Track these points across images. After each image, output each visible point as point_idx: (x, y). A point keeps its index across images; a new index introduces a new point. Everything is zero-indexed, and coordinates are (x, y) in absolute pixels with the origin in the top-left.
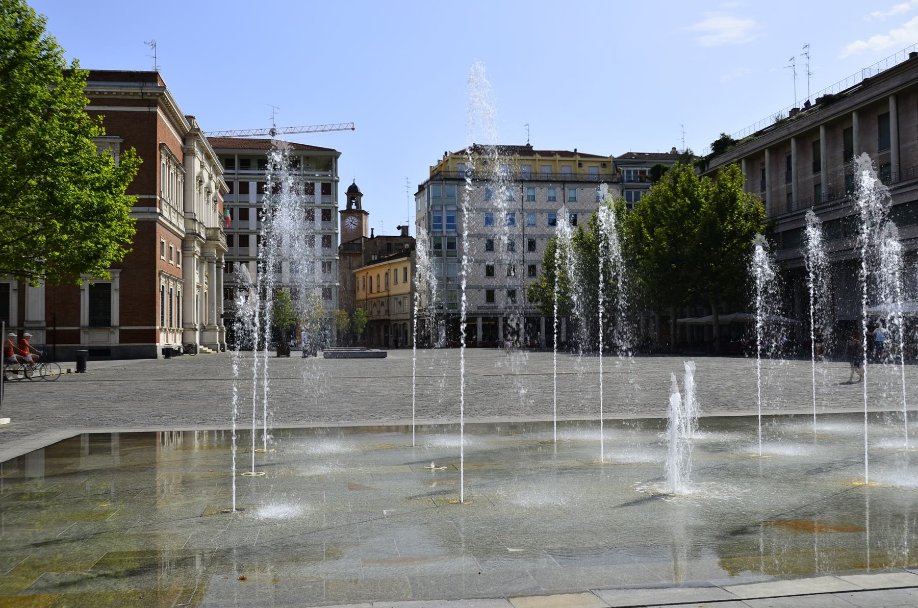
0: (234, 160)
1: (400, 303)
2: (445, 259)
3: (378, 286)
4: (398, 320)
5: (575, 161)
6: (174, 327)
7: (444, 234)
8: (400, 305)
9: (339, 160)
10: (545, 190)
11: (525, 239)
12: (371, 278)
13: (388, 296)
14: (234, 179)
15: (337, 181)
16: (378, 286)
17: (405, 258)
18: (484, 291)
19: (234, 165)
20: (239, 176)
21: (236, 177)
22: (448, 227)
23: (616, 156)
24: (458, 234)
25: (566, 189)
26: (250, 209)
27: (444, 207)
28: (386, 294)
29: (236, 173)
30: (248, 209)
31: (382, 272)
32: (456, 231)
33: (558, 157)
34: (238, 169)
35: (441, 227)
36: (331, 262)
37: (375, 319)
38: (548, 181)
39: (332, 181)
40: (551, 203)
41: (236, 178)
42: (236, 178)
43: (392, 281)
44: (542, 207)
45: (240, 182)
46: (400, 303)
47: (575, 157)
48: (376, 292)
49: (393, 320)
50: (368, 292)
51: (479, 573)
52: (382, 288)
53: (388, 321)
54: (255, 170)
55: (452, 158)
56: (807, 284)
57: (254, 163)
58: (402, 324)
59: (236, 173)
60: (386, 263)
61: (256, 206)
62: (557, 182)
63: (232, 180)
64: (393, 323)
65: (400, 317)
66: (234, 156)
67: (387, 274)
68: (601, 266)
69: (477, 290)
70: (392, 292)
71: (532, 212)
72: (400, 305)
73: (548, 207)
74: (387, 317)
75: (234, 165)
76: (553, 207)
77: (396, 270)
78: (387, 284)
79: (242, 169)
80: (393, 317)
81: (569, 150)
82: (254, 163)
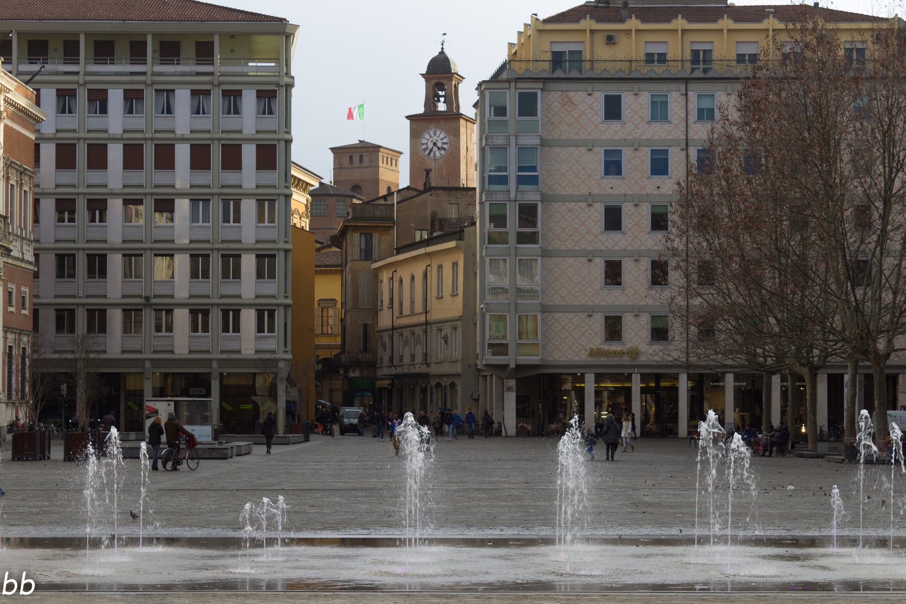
0: (145, 43)
1: (446, 339)
2: (513, 251)
3: (412, 302)
4: (440, 376)
5: (768, 30)
7: (513, 196)
8: (446, 342)
12: (401, 281)
13: (427, 323)
14: (145, 83)
15: (289, 86)
16: (412, 302)
17: (452, 244)
18: (599, 318)
19: (78, 55)
20: (88, 78)
21: (81, 79)
22: (521, 180)
23: (737, 5)
24: (542, 195)
25: (690, 93)
26: (109, 146)
27: (513, 139)
28: (422, 319)
29: (149, 72)
30: (106, 145)
31: (418, 270)
33: (772, 23)
34: (153, 64)
35: (504, 180)
36: (274, 256)
37: (406, 371)
39: (278, 85)
41: (81, 82)
42: (81, 82)
43: (433, 292)
45: (89, 90)
46: (446, 339)
47: (766, 21)
48: (408, 313)
49: (435, 376)
50: (396, 314)
52: (419, 307)
53: (426, 376)
54: (188, 64)
55: (540, 31)
57: (123, 49)
58: (448, 383)
60: (421, 251)
61: (122, 139)
64: (433, 383)
65: (446, 369)
67: (425, 275)
68: (164, 438)
69: (583, 316)
70: (434, 316)
72: (446, 342)
74: (424, 369)
75: (145, 55)
77: (440, 267)
78: (425, 300)
80: (434, 370)
81: (747, 5)
82: (123, 49)
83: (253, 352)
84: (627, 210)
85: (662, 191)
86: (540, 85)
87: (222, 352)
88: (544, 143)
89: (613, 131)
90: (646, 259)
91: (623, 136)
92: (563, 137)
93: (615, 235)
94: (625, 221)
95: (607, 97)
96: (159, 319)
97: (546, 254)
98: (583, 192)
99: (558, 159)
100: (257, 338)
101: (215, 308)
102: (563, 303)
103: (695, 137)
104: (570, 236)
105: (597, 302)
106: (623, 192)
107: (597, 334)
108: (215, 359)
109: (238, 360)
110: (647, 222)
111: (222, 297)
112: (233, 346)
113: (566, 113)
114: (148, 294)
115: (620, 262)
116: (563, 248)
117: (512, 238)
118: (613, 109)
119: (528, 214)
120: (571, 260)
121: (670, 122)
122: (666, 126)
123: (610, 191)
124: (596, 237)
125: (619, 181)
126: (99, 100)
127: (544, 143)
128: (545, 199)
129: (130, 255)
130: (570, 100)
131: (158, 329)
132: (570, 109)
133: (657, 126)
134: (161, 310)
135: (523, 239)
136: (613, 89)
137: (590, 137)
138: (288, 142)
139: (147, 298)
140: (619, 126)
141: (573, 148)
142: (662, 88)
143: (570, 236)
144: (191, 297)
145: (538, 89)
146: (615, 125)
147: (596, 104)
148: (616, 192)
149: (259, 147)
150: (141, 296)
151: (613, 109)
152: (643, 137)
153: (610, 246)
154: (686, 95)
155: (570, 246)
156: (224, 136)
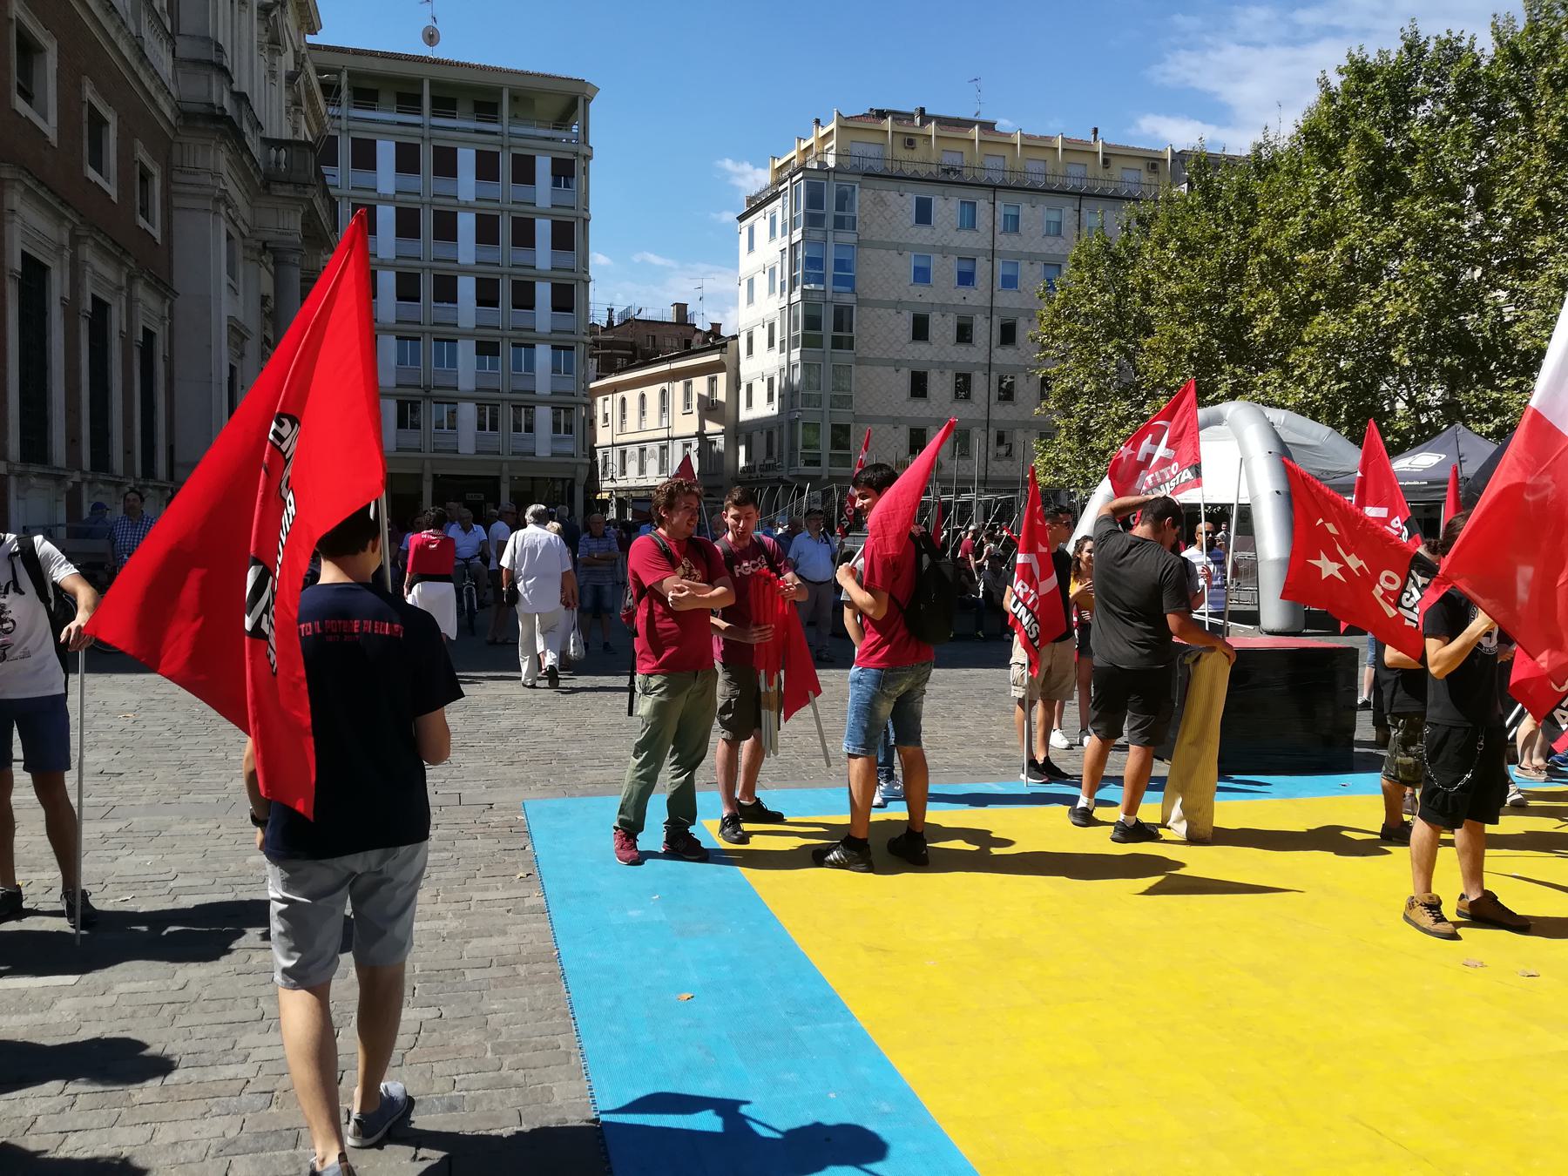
6: (615, 457)
7: (829, 296)
9: (592, 106)
10: (1041, 210)
11: (995, 317)
15: (587, 158)
25: (1083, 209)
29: (427, 124)
32: (853, 291)
36: (572, 348)
38: (1048, 191)
39: (577, 154)
40: (1050, 240)
44: (1031, 248)
51: (828, 1140)
56: (731, 601)
59: (344, 115)
62: (1062, 192)
63: (497, 149)
66: (420, 82)
69: (890, 427)
71: (1015, 259)
73: (1044, 249)
76: (1056, 249)
79: (435, 114)
83: (549, 455)
84: (935, 320)
85: (968, 302)
86: (859, 178)
87: (514, 454)
88: (860, 243)
89: (922, 235)
90: (951, 371)
91: (932, 242)
92: (874, 238)
93: (922, 346)
94: (933, 332)
95: (918, 199)
96: (481, 415)
97: (860, 361)
98: (893, 298)
99: (868, 262)
100: (554, 440)
101: (506, 403)
102: (871, 414)
103: (1001, 249)
104: (879, 344)
105: (903, 414)
106: (931, 301)
107: (902, 446)
108: (505, 461)
109: (455, 460)
110: (952, 334)
111: (514, 391)
112: (527, 447)
113: (878, 213)
114: (427, 383)
115: (925, 373)
116: (871, 356)
117: (828, 342)
118: (924, 214)
119: (843, 318)
120: (879, 369)
121: (977, 231)
122: (975, 234)
123: (919, 299)
124: (904, 346)
125: (928, 289)
126: (446, 164)
127: (860, 243)
128: (860, 303)
129: (406, 338)
130: (882, 200)
131: (517, 428)
132: (881, 209)
133: (965, 234)
134: (521, 407)
135: (837, 343)
136: (925, 191)
137: (901, 241)
138: (586, 221)
139: (427, 388)
140: (929, 231)
141: (884, 251)
142: (971, 194)
143: (879, 344)
144: (478, 390)
145: (856, 182)
146: (925, 230)
147: (908, 206)
148: (924, 301)
149: (400, 212)
150: (419, 387)
151: (924, 214)
152: (952, 245)
153: (917, 357)
154: (1079, 211)
155: (878, 355)
156: (515, 207)
